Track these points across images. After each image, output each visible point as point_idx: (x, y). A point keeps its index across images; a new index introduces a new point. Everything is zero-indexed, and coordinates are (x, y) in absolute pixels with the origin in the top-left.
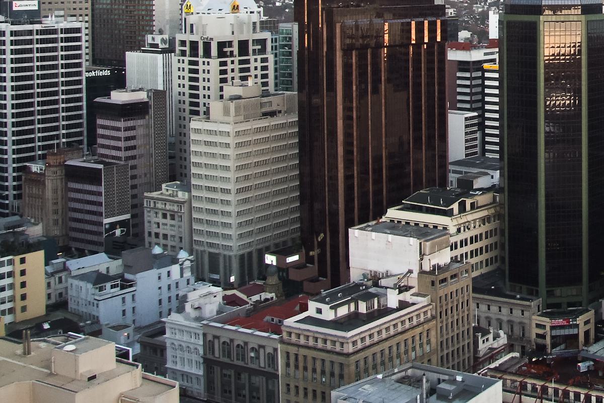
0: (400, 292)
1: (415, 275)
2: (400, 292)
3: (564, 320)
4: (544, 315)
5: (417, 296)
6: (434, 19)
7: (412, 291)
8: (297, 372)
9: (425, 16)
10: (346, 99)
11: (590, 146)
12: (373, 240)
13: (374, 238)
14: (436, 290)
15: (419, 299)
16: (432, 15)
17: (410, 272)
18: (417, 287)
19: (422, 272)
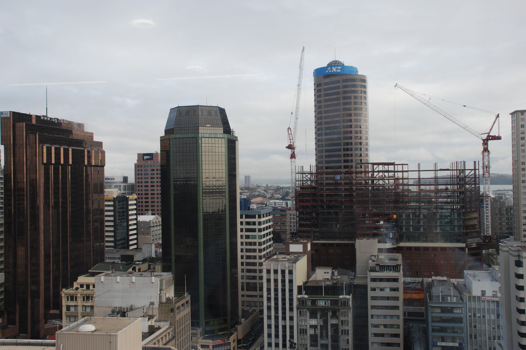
0: (149, 319)
1: (156, 305)
2: (149, 319)
3: (221, 340)
4: (205, 338)
5: (160, 322)
6: (67, 147)
7: (155, 318)
8: (439, 311)
9: (61, 144)
10: (287, 198)
11: (175, 215)
12: (118, 282)
13: (118, 280)
14: (174, 315)
15: (162, 324)
16: (58, 144)
17: (152, 304)
18: (157, 315)
19: (161, 303)
